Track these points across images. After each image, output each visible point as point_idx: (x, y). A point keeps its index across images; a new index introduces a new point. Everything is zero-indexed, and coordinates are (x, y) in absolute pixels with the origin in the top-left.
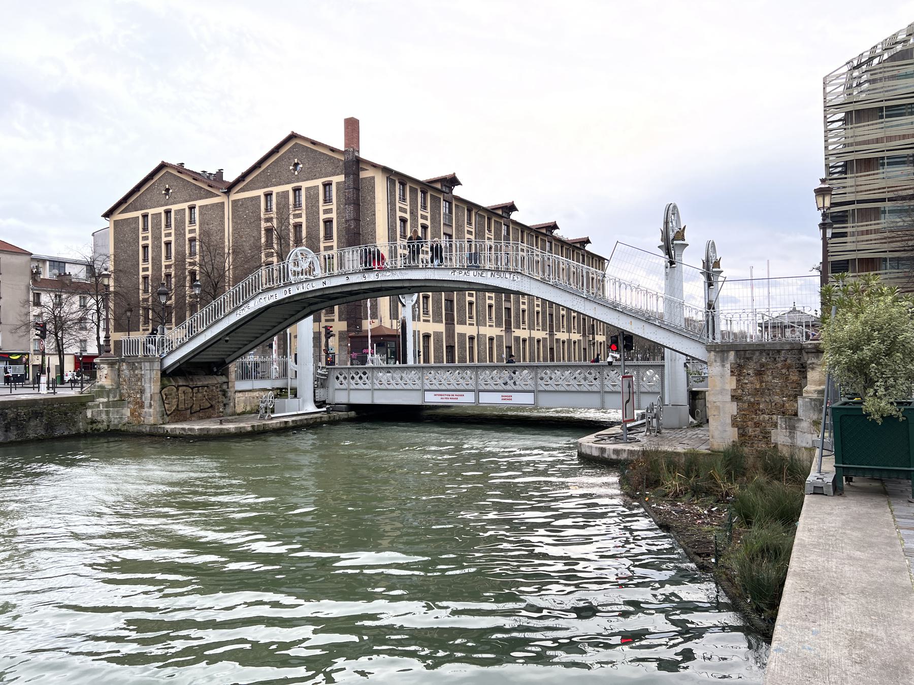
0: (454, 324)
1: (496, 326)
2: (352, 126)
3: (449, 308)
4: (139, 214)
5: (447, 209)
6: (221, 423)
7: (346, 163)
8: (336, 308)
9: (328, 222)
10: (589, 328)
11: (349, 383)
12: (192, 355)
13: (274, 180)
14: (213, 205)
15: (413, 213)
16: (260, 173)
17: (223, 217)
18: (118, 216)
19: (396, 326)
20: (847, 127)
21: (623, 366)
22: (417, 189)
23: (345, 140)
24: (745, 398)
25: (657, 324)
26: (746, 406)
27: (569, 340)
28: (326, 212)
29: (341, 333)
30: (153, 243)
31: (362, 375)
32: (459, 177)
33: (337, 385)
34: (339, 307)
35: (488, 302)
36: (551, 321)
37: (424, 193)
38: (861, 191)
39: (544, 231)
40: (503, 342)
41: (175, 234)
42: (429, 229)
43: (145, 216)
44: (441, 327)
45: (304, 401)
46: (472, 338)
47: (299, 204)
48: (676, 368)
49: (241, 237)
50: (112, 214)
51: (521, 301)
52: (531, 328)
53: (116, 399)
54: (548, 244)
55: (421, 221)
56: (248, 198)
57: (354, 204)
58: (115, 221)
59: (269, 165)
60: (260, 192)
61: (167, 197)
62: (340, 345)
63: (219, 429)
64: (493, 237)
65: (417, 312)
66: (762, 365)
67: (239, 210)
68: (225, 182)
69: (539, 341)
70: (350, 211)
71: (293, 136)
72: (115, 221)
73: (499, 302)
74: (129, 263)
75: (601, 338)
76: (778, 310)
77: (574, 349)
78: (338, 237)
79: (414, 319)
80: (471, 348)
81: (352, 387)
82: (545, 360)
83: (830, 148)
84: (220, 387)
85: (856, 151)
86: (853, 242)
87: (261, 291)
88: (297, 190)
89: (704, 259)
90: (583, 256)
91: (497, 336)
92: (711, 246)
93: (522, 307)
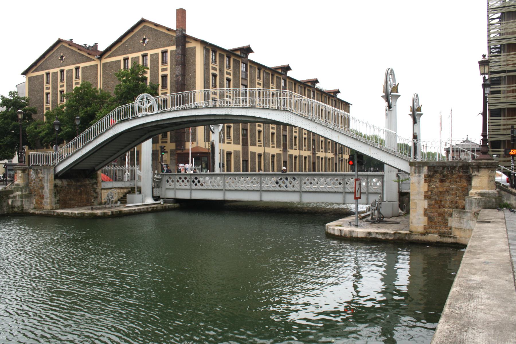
0: (247, 145)
1: (277, 147)
2: (181, 14)
3: (245, 136)
4: (44, 73)
5: (244, 69)
6: (92, 209)
7: (177, 38)
8: (169, 133)
9: (164, 77)
10: (339, 149)
11: (175, 185)
12: (74, 164)
14: (90, 66)
15: (221, 71)
16: (121, 45)
17: (97, 74)
19: (208, 146)
20: (501, 22)
21: (356, 175)
22: (224, 56)
23: (177, 23)
24: (433, 197)
25: (379, 147)
26: (433, 202)
27: (326, 158)
28: (163, 70)
29: (171, 151)
30: (52, 91)
31: (184, 180)
32: (319, 80)
33: (168, 186)
34: (170, 133)
35: (271, 131)
36: (314, 144)
37: (229, 57)
38: (510, 65)
39: (309, 84)
40: (281, 158)
42: (232, 82)
43: (48, 74)
44: (239, 148)
45: (145, 196)
46: (260, 155)
48: (390, 176)
49: (108, 87)
51: (294, 130)
52: (301, 149)
53: (26, 193)
54: (312, 93)
55: (226, 76)
56: (113, 62)
59: (127, 40)
60: (121, 58)
61: (62, 62)
62: (171, 159)
63: (90, 213)
64: (275, 87)
65: (222, 137)
66: (444, 176)
67: (107, 69)
68: (99, 51)
69: (305, 158)
71: (143, 21)
73: (278, 130)
74: (38, 105)
75: (346, 157)
76: (457, 140)
77: (329, 164)
79: (220, 142)
80: (260, 162)
81: (177, 187)
82: (309, 171)
83: (492, 36)
84: (92, 186)
85: (507, 39)
86: (504, 97)
87: (117, 123)
88: (145, 56)
89: (411, 105)
90: (335, 101)
91: (277, 154)
92: (416, 98)
93: (294, 134)
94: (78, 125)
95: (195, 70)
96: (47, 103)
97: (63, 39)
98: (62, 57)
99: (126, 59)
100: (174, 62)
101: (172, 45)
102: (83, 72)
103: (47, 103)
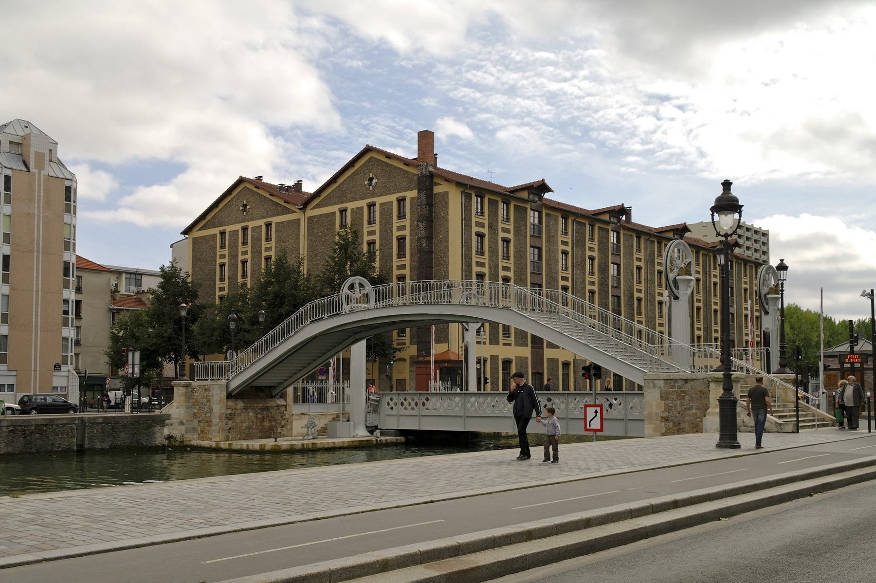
0: (542, 348)
2: (426, 139)
4: (216, 231)
7: (420, 178)
8: (408, 330)
9: (401, 240)
13: (349, 196)
14: (289, 222)
15: (493, 227)
16: (336, 189)
17: (299, 235)
18: (196, 234)
22: (497, 202)
31: (411, 401)
41: (252, 252)
43: (223, 233)
47: (374, 221)
50: (191, 231)
55: (501, 235)
57: (427, 220)
58: (194, 239)
60: (335, 209)
61: (245, 214)
70: (422, 231)
71: (368, 150)
72: (194, 239)
76: (207, 356)
78: (411, 255)
88: (371, 206)
94: (263, 322)
95: (447, 228)
96: (222, 279)
97: (247, 177)
98: (245, 206)
99: (343, 211)
100: (416, 216)
101: (412, 189)
102: (277, 231)
103: (222, 279)
